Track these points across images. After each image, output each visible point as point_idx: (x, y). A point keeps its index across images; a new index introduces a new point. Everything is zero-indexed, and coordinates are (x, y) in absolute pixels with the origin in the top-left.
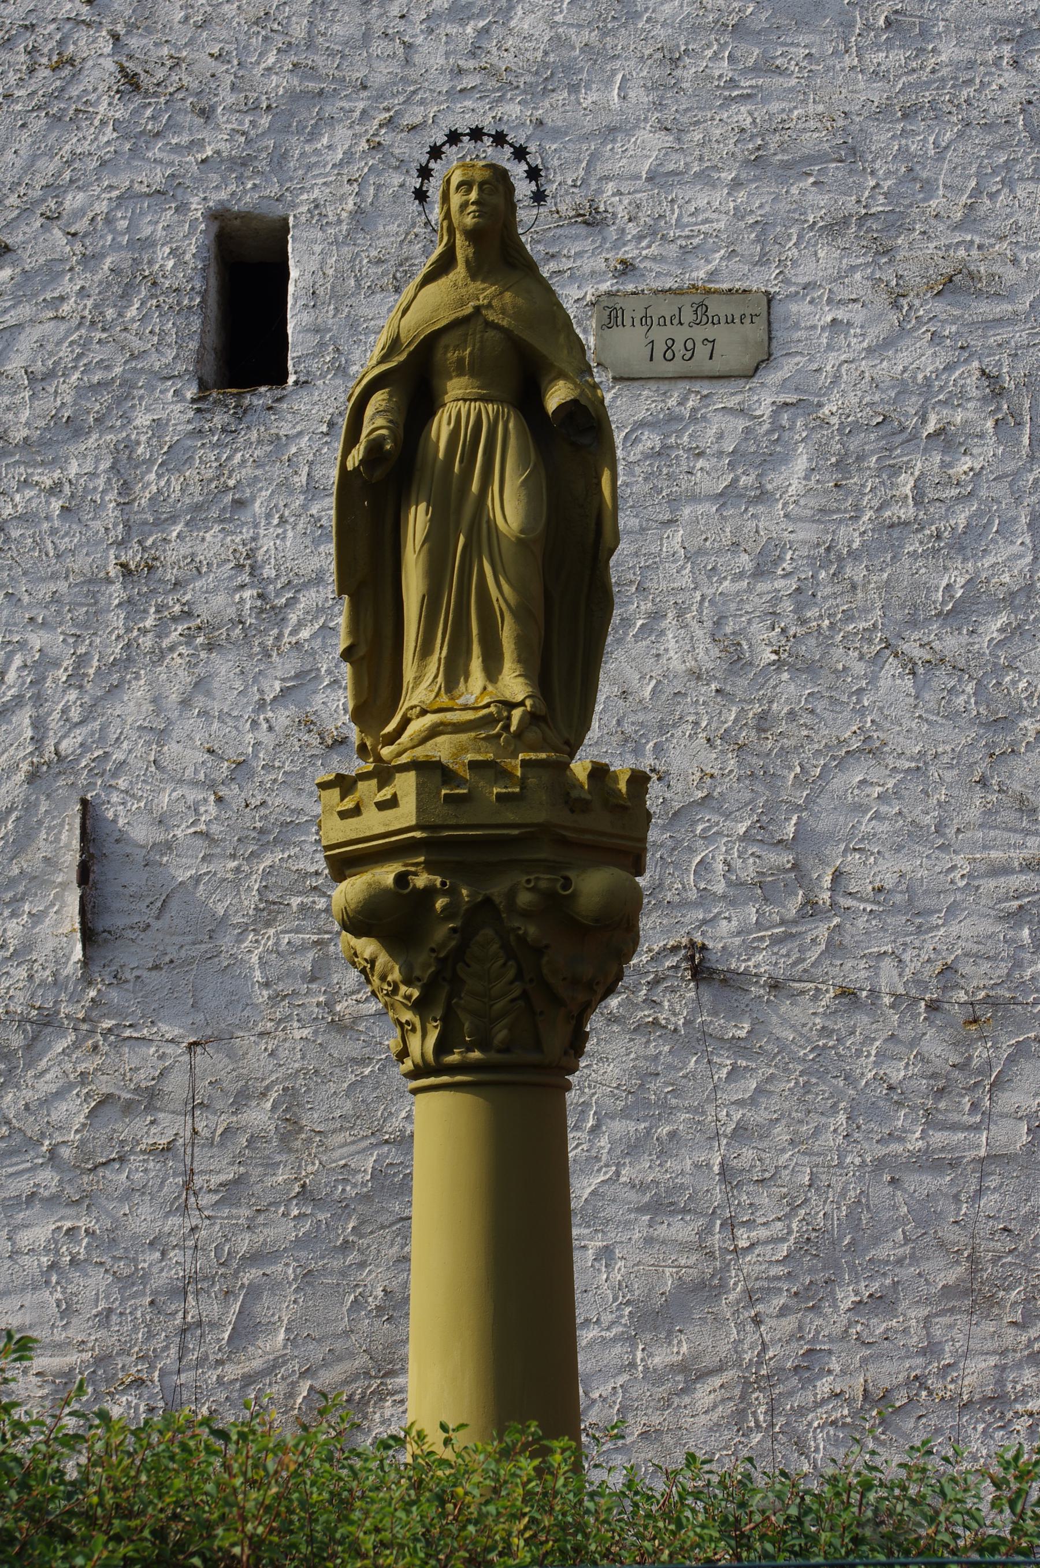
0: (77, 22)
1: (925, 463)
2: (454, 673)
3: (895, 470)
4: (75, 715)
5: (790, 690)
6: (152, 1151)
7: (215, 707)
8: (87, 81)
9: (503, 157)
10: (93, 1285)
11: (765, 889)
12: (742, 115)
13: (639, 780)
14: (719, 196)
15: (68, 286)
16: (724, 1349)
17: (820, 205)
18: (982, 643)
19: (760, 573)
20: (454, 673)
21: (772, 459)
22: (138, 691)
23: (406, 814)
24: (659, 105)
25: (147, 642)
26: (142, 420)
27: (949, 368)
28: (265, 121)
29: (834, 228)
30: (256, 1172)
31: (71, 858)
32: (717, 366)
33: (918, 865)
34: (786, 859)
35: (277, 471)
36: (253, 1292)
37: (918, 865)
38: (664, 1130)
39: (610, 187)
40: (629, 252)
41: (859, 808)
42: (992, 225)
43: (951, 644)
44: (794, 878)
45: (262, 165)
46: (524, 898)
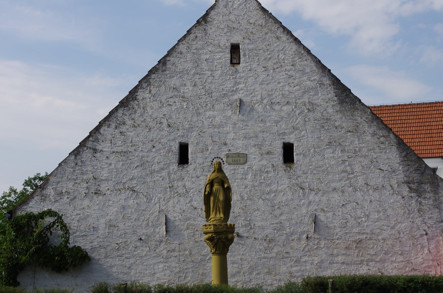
0: (162, 118)
1: (265, 175)
2: (216, 214)
3: (261, 176)
4: (164, 204)
5: (249, 202)
6: (174, 256)
7: (181, 204)
8: (164, 125)
9: (221, 161)
10: (168, 272)
11: (246, 226)
12: (243, 131)
13: (234, 225)
14: (241, 142)
15: (162, 151)
16: (241, 279)
17: (253, 143)
18: (271, 197)
19: (245, 188)
20: (216, 214)
21: (247, 174)
22: (172, 202)
23: (212, 229)
24: (233, 130)
25: (172, 196)
26: (171, 168)
27: (268, 163)
28: (186, 131)
29: (255, 146)
30: (186, 259)
31: (164, 221)
32: (240, 163)
33: (263, 223)
34: (248, 222)
35: (188, 175)
36: (186, 273)
37: (263, 223)
38: (234, 254)
39: (228, 140)
40: (230, 148)
41: (257, 216)
42: (273, 146)
43: (268, 197)
44: (249, 225)
45: (185, 136)
46: (223, 237)
